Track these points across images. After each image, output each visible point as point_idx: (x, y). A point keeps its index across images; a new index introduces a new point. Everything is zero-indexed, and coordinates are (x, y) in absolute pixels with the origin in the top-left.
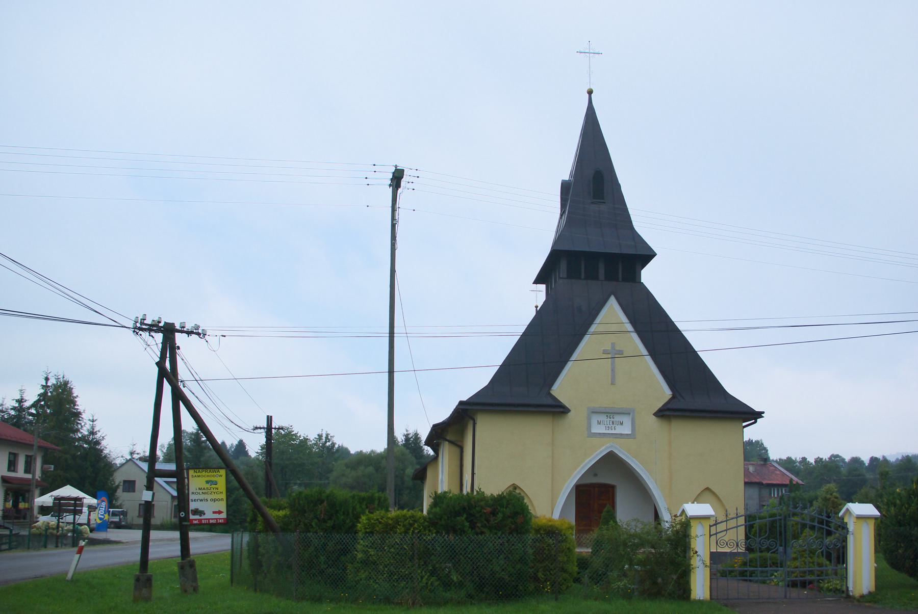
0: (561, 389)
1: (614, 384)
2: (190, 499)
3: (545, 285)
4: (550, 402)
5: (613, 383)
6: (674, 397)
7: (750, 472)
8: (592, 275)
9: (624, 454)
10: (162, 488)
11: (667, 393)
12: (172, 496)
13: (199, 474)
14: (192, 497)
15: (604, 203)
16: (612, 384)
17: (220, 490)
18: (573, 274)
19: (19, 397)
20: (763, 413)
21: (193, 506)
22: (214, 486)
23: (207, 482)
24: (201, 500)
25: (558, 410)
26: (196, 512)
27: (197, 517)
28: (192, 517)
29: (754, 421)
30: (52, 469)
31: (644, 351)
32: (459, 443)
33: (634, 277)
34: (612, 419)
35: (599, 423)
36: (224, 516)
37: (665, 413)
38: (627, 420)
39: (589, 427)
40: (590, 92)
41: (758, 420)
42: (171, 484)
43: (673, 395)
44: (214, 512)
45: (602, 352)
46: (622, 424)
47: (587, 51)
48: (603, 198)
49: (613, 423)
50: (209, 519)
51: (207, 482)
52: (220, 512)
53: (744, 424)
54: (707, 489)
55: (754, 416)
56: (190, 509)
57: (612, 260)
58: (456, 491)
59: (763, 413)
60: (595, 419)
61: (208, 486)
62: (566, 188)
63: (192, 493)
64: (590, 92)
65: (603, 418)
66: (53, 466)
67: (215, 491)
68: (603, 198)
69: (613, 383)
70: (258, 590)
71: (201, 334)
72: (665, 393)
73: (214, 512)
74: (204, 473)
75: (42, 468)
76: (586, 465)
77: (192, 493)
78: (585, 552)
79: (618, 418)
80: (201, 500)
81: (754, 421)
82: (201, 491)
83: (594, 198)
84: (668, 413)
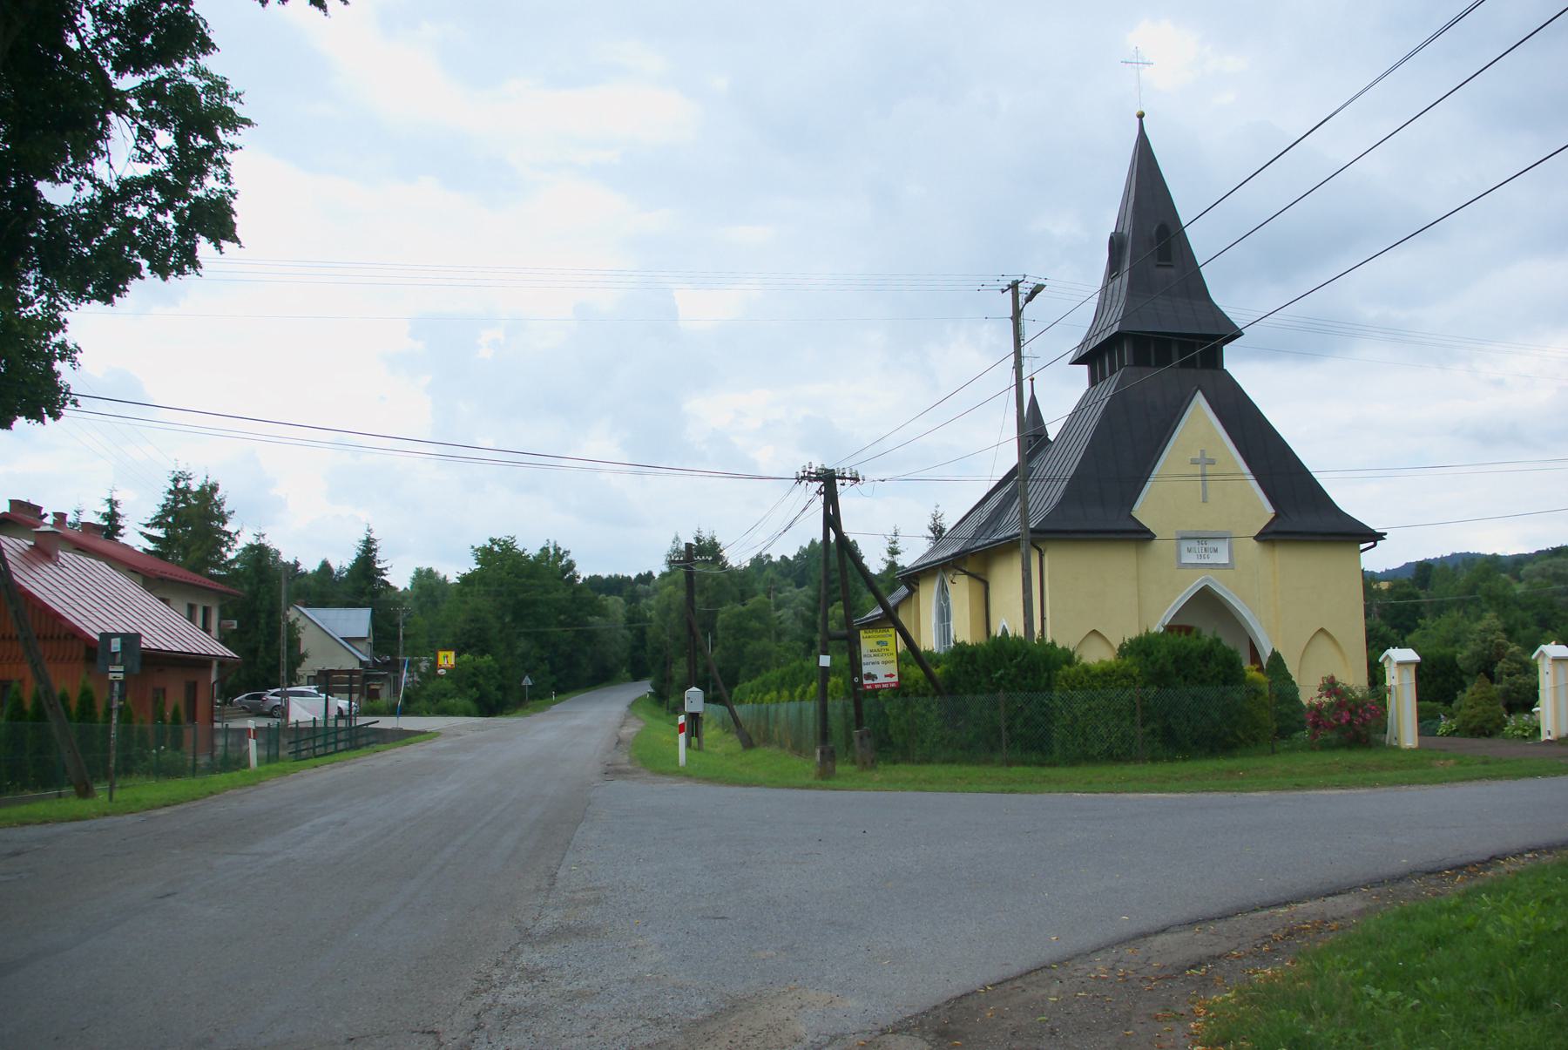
0: (1145, 510)
1: (1206, 502)
2: (896, 664)
3: (1086, 366)
4: (1132, 526)
5: (1204, 501)
6: (1277, 516)
7: (863, 570)
8: (1163, 360)
9: (1221, 588)
10: (345, 651)
11: (1269, 511)
12: (361, 661)
13: (870, 634)
14: (864, 660)
15: (1171, 266)
16: (1203, 502)
17: (890, 651)
18: (1140, 361)
19: (107, 509)
20: (1385, 534)
21: (866, 670)
22: (884, 647)
23: (878, 643)
24: (873, 663)
25: (1141, 536)
26: (870, 676)
27: (870, 682)
28: (865, 682)
29: (1372, 543)
30: (235, 627)
31: (1244, 468)
32: (983, 577)
33: (1213, 360)
34: (1204, 546)
35: (1189, 551)
36: (895, 679)
37: (1268, 536)
38: (1223, 547)
39: (1179, 556)
40: (1141, 116)
41: (1378, 542)
42: (352, 643)
43: (1276, 513)
44: (886, 676)
45: (1190, 461)
46: (1216, 551)
47: (1140, 65)
48: (1169, 260)
49: (1205, 550)
50: (881, 684)
51: (878, 643)
52: (891, 676)
53: (1363, 546)
54: (1094, 631)
55: (1376, 537)
56: (864, 673)
57: (1188, 342)
58: (981, 638)
59: (1385, 534)
60: (1185, 545)
61: (879, 647)
62: (1468, 553)
63: (865, 656)
64: (1141, 116)
65: (1194, 544)
66: (235, 622)
67: (886, 652)
68: (1169, 260)
69: (1204, 501)
70: (1442, 716)
71: (81, 352)
72: (1266, 511)
73: (886, 676)
74: (874, 634)
75: (219, 624)
76: (1175, 606)
77: (865, 656)
78: (195, 771)
79: (1211, 544)
80: (873, 663)
81: (1372, 543)
82: (872, 654)
83: (1160, 260)
84: (1273, 537)
